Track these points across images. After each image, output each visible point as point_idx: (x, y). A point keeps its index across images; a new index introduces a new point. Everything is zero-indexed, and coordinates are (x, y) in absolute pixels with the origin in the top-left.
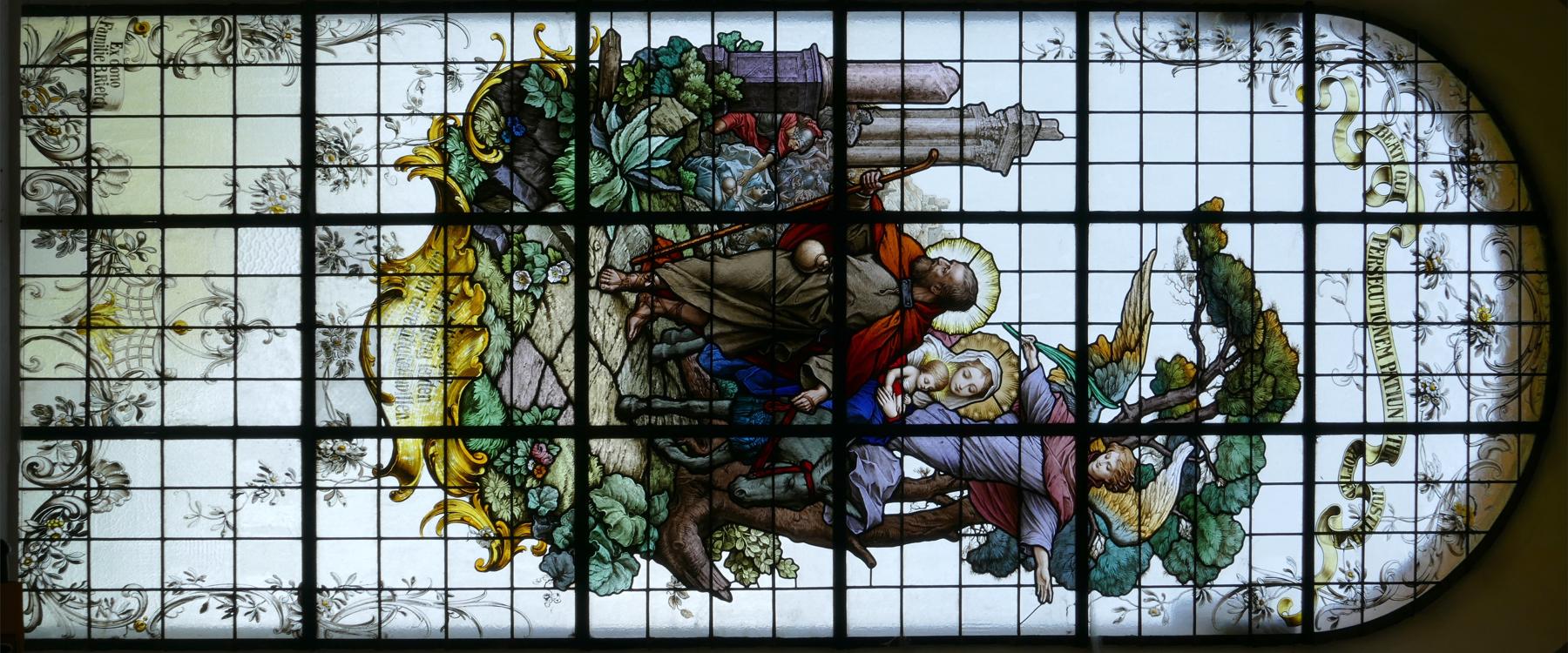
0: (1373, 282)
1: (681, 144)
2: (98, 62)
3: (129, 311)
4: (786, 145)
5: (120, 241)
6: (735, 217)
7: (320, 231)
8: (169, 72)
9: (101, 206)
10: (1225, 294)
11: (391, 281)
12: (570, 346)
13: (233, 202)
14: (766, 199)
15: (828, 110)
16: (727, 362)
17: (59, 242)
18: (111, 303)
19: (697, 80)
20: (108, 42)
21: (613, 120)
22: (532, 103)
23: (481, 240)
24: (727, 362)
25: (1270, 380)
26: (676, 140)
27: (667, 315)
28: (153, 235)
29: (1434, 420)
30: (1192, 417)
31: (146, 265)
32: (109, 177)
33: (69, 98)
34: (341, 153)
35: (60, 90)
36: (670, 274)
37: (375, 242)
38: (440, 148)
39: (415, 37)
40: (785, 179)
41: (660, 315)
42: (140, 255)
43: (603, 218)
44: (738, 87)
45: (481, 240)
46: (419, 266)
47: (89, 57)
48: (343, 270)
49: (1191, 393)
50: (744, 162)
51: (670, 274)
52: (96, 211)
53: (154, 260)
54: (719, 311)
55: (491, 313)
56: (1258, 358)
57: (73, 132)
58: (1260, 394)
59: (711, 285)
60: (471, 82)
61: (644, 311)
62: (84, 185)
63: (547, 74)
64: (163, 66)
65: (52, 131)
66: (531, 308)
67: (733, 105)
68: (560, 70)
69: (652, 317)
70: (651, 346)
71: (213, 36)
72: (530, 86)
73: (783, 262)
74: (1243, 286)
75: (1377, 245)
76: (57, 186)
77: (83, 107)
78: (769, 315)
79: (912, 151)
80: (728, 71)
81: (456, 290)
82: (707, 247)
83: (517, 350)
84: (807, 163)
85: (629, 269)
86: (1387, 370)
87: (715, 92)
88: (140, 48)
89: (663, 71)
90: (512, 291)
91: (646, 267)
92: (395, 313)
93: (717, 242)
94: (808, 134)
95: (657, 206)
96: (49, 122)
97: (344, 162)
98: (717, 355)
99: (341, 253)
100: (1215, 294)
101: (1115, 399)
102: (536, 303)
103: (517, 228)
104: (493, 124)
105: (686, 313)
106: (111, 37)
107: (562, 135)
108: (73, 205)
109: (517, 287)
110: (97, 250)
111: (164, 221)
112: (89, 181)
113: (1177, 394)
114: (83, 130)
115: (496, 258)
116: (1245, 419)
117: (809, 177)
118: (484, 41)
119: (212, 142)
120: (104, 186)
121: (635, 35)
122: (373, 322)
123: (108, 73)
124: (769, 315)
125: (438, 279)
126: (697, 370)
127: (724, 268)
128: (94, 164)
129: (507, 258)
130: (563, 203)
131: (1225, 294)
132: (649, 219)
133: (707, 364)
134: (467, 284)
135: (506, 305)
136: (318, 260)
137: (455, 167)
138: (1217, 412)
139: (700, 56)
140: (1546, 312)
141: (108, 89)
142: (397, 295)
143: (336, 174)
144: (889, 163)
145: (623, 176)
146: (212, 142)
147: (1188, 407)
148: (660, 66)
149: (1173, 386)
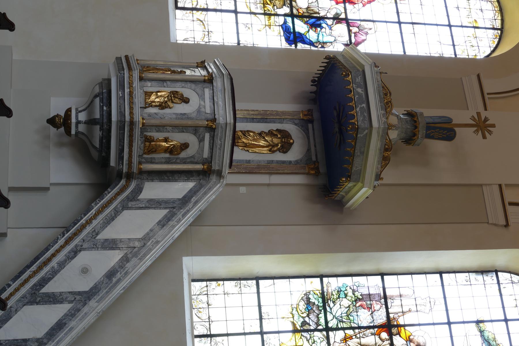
1: (349, 310)
14: (371, 323)
19: (350, 294)
21: (332, 305)
23: (304, 336)
40: (375, 317)
43: (332, 329)
45: (304, 336)
68: (317, 292)
72: (311, 296)
82: (358, 336)
94: (379, 306)
95: (345, 326)
103: (312, 333)
112: (210, 325)
115: (308, 341)
117: (380, 318)
129: (310, 341)
132: (344, 329)
139: (350, 288)
144: (399, 313)
148: (341, 291)
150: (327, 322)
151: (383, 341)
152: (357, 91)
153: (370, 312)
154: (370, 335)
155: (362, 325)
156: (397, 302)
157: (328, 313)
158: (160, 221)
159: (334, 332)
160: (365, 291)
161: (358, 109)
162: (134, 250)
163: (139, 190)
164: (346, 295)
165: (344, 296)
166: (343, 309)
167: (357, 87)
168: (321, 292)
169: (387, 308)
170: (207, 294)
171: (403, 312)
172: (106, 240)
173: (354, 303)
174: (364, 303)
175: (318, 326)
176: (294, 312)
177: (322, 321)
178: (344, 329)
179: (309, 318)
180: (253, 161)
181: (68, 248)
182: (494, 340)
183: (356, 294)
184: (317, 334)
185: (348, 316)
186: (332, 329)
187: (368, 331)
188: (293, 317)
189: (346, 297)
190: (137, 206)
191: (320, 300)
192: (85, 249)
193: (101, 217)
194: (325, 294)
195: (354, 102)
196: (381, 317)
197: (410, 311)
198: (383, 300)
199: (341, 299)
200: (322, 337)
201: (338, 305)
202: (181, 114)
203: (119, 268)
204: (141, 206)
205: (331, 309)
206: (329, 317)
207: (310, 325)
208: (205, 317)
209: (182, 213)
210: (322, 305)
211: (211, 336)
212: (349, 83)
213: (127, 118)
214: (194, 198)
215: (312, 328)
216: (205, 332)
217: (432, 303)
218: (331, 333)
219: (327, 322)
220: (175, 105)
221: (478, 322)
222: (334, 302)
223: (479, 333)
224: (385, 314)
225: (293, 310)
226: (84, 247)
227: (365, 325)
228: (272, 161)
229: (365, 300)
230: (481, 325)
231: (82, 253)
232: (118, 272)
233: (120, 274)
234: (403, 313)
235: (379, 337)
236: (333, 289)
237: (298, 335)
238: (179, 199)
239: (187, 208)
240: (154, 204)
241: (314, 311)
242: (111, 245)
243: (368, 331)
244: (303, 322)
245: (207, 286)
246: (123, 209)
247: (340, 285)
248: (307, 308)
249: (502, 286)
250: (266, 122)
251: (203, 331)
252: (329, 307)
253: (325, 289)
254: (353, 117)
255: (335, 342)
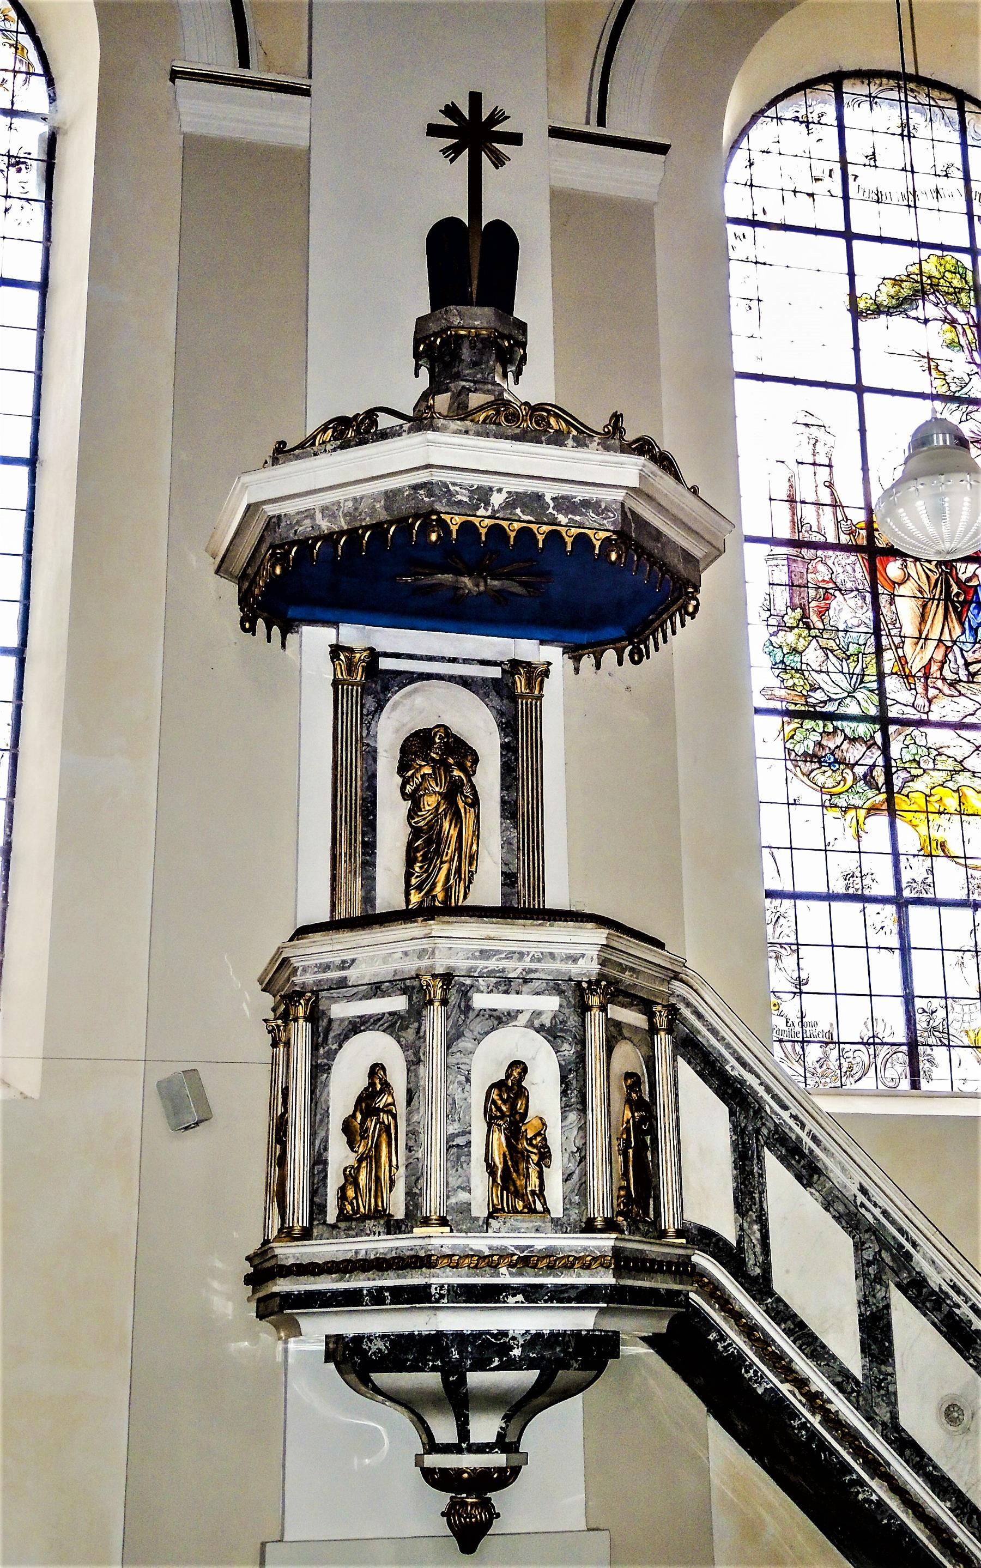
0: (884, 197)
1: (832, 651)
2: (800, 1035)
3: (972, 1020)
4: (828, 582)
5: (925, 1025)
6: (877, 622)
7: (906, 893)
8: (804, 988)
9: (901, 1036)
10: (909, 296)
11: (934, 849)
12: (963, 733)
13: (891, 949)
14: (864, 598)
15: (804, 551)
16: (967, 632)
17: (928, 1065)
18: (967, 1032)
19: (791, 637)
20: (786, 1029)
21: (819, 695)
22: (811, 748)
23: (902, 788)
24: (967, 632)
25: (947, 274)
26: (830, 654)
27: (941, 669)
28: (919, 1003)
29: (961, 167)
30: (974, 329)
31: (940, 1009)
32: (879, 1029)
33: (826, 1057)
34: (852, 876)
35: (822, 1061)
36: (916, 666)
37: (910, 858)
38: (845, 810)
39: (772, 826)
40: (849, 585)
41: (941, 674)
42: (933, 1012)
43: (883, 706)
44: (793, 610)
45: (902, 788)
46: (923, 829)
47: (797, 1041)
48: (930, 880)
49: (959, 328)
50: (840, 610)
51: (916, 666)
52: (904, 1040)
53: (936, 1003)
54: (935, 634)
55: (949, 784)
56: (935, 281)
57: (850, 1054)
58: (957, 283)
59: (922, 639)
60: (800, 789)
61: (939, 683)
62: (886, 1047)
63: (792, 737)
64: (801, 993)
65: (850, 1068)
66: (944, 757)
67: (804, 616)
68: (788, 729)
69: (944, 679)
70: (961, 681)
71: (777, 958)
72: (800, 749)
73: (902, 590)
74: (894, 285)
75: (861, 191)
76: (889, 1065)
77: (832, 1046)
78: (936, 602)
79: (827, 499)
80: (783, 617)
81: (937, 805)
82: (897, 640)
83: (971, 769)
84: (840, 570)
85: (914, 692)
86: (935, 195)
87: (797, 626)
88: (790, 1007)
89: (785, 660)
90: (934, 769)
91: (911, 680)
92: (955, 848)
93: (892, 633)
94: (820, 567)
95: (872, 670)
96: (844, 1070)
97: (859, 875)
98: (962, 638)
99: (919, 880)
100: (900, 305)
101: (967, 380)
102: (940, 754)
103: (893, 764)
104: (827, 774)
105: (939, 656)
106: (782, 1026)
107: (831, 730)
108: (900, 1055)
109: (931, 766)
110: (932, 1041)
111: (909, 998)
112: (883, 1044)
113: (961, 336)
114: (847, 1047)
115: (914, 778)
116: (972, 294)
117: (850, 570)
118: (772, 778)
119: (851, 961)
120: (886, 1034)
121: (762, 678)
122: (962, 861)
123: (808, 1029)
124: (936, 602)
125: (931, 816)
126: (974, 652)
127: (910, 628)
128: (871, 1041)
129: (914, 772)
130: (874, 732)
131: (909, 296)
132: (881, 676)
133: (970, 646)
134: (931, 799)
135: (944, 774)
136: (925, 896)
137: (858, 802)
138: (969, 312)
139: (775, 634)
140: (892, 83)
141: (819, 1029)
142: (943, 845)
143: (867, 881)
144: (835, 514)
145: (854, 692)
146: (851, 961)
147: (968, 332)
148: (782, 662)
149: (956, 340)
150: (864, 718)
151: (907, 577)
152: (502, 508)
153: (837, 593)
154: (893, 607)
155: (871, 624)
156: (809, 514)
157: (842, 710)
158: (799, 1178)
159: (889, 702)
160: (782, 597)
161: (562, 519)
162: (885, 1260)
163: (705, 1238)
164: (794, 651)
165: (797, 658)
166: (831, 668)
167: (487, 504)
168: (786, 719)
169: (825, 546)
170: (803, 1042)
171: (835, 506)
172: (865, 1349)
173: (813, 632)
174: (813, 604)
175: (875, 743)
176: (842, 802)
177: (863, 729)
178: (881, 676)
179: (856, 764)
180: (505, 863)
181: (899, 1467)
182: (896, 282)
183: (790, 621)
184: (895, 752)
185: (849, 657)
186: (883, 706)
187: (884, 611)
188: (856, 808)
189: (801, 653)
190: (758, 1249)
191: (808, 724)
192: (894, 1416)
193: (803, 1365)
194: (792, 707)
195: (534, 527)
196: (849, 568)
197: (830, 485)
198: (808, 553)
199: (804, 667)
200: (901, 738)
201: (820, 679)
202: (564, 1093)
203: (939, 1310)
204: (758, 1235)
205: (831, 700)
206: (852, 709)
207: (874, 766)
208: (863, 1055)
209: (777, 1108)
210: (821, 723)
211: (913, 1046)
212: (468, 528)
213: (606, 1278)
214: (728, 1068)
215: (881, 761)
216: (903, 1058)
217: (810, 420)
218: (893, 712)
219: (864, 718)
220: (531, 1113)
221: (856, 314)
222: (814, 689)
223: (883, 317)
224: (841, 555)
225: (836, 806)
226: (887, 1418)
227: (870, 614)
228: (503, 802)
229: (804, 601)
230: (862, 305)
231: (904, 1422)
232: (951, 1314)
233: (959, 1307)
234: (836, 505)
235: (899, 584)
236: (777, 682)
237: (901, 803)
238: (732, 1113)
239: (761, 1091)
240: (748, 1194)
241: (837, 747)
242: (876, 1332)
243: (885, 610)
244: (866, 783)
245: (780, 1041)
246: (771, 1293)
247: (767, 661)
248: (830, 765)
249: (760, 217)
250: (374, 803)
251: (898, 1068)
252: (825, 702)
253: (778, 705)
254: (582, 541)
255: (913, 706)
